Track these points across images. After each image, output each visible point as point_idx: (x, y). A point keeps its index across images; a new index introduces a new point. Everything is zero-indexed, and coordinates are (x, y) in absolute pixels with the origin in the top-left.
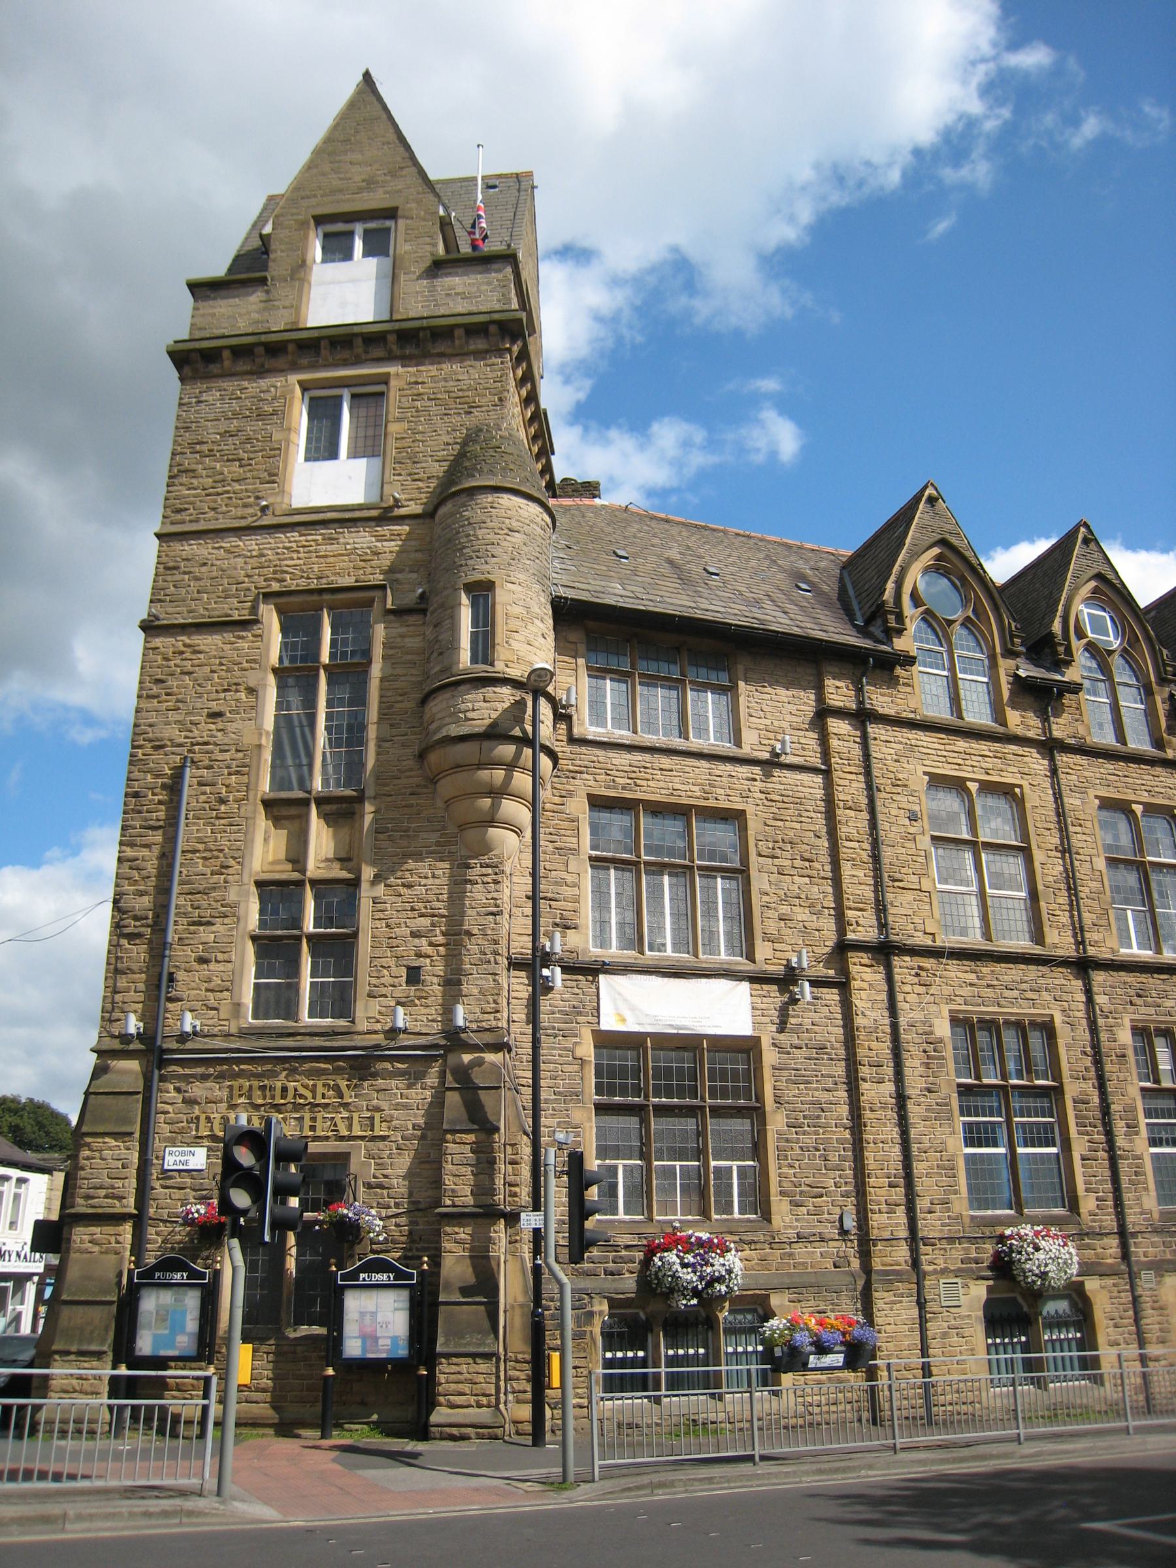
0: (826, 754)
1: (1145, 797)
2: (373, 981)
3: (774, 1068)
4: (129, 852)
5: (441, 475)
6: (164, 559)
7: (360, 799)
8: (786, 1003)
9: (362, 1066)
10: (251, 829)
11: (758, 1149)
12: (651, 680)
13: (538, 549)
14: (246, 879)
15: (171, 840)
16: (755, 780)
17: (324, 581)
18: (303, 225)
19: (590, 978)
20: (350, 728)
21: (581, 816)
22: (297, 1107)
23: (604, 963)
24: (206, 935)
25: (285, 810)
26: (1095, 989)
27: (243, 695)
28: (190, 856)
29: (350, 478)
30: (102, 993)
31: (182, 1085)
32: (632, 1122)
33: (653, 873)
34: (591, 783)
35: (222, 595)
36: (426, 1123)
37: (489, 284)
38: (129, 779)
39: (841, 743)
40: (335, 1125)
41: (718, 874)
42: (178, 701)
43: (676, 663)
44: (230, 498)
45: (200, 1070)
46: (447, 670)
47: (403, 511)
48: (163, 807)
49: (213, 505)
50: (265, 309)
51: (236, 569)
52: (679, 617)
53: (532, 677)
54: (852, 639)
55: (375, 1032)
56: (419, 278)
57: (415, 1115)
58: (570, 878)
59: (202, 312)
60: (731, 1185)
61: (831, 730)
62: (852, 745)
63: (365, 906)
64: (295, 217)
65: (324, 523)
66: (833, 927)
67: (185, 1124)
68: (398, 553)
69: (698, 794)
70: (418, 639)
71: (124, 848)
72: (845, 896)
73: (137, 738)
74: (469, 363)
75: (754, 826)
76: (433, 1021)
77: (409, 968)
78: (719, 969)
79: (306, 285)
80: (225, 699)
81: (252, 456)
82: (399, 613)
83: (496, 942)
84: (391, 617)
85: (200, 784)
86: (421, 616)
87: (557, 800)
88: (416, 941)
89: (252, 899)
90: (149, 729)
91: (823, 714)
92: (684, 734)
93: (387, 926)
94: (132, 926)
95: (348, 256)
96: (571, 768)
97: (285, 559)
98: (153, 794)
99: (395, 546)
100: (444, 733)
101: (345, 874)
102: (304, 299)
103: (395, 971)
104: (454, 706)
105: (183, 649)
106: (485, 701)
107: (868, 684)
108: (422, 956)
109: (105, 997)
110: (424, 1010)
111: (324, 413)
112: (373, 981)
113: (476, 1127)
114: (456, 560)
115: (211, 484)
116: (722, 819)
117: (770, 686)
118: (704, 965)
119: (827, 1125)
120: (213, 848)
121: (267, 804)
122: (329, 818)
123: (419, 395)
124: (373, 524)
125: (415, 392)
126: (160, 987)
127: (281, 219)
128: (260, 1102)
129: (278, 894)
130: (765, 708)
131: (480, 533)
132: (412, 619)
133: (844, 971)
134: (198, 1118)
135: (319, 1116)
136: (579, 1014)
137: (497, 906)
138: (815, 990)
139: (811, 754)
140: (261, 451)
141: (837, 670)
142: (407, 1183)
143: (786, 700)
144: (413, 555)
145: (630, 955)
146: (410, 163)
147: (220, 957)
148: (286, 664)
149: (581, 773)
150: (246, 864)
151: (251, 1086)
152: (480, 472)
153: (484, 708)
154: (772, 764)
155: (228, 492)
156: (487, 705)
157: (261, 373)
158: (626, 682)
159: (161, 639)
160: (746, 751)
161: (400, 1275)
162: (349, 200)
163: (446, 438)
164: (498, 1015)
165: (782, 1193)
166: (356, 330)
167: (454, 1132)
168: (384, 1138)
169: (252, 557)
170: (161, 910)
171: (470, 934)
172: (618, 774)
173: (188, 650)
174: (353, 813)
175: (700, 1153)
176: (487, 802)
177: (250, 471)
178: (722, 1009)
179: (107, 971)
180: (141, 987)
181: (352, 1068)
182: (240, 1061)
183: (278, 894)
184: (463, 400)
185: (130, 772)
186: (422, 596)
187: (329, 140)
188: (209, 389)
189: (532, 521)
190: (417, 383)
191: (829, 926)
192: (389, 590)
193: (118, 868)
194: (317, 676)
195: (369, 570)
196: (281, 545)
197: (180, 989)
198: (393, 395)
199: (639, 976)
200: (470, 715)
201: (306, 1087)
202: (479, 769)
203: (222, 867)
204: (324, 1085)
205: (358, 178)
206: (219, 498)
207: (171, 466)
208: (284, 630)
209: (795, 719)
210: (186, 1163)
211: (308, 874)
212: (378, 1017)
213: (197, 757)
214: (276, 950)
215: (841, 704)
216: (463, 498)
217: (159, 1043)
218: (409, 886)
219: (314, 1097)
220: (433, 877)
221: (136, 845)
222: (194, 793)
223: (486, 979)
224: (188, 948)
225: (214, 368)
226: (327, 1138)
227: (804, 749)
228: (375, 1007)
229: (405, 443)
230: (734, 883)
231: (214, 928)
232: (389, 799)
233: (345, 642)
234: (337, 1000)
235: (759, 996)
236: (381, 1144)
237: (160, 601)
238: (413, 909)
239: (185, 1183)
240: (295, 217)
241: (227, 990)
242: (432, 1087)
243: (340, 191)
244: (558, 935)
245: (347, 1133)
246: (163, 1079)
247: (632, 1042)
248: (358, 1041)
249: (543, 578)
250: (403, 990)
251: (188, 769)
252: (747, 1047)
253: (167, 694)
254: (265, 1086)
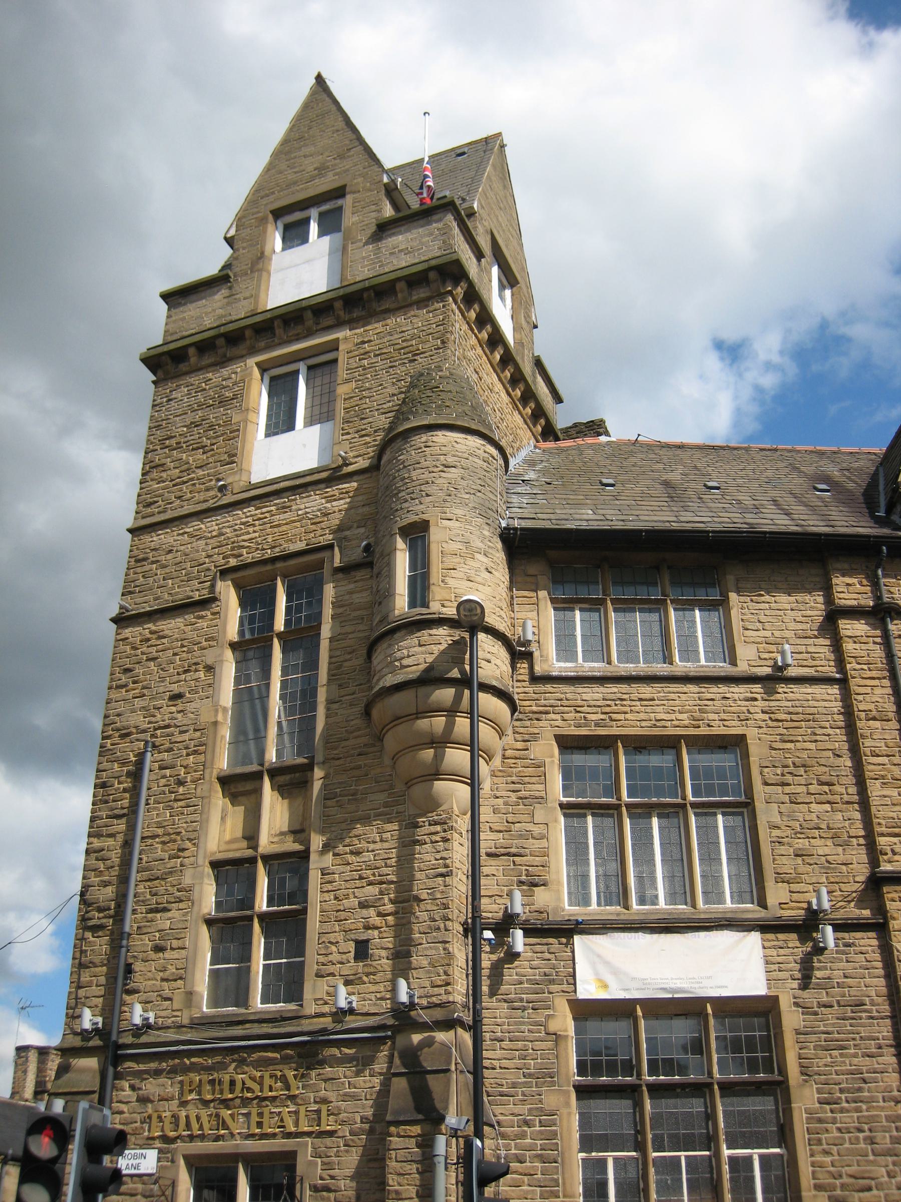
0: (840, 662)
2: (322, 959)
3: (798, 1032)
4: (97, 843)
5: (387, 426)
6: (136, 552)
7: (309, 767)
8: (809, 953)
9: (309, 1053)
10: (206, 810)
11: (784, 1134)
12: (624, 606)
13: (479, 482)
14: (200, 861)
15: (132, 827)
16: (756, 699)
17: (277, 549)
18: (263, 221)
19: (564, 940)
20: (303, 692)
21: (547, 760)
22: (245, 1102)
23: (578, 923)
24: (163, 922)
25: (240, 786)
27: (201, 674)
28: (150, 841)
29: (304, 445)
30: (68, 989)
31: (136, 1082)
32: (623, 1106)
33: (640, 816)
34: (560, 723)
35: (185, 578)
36: (374, 1115)
37: (431, 234)
38: (98, 771)
39: (857, 646)
40: (282, 1120)
41: (719, 811)
42: (144, 688)
43: (656, 584)
44: (194, 485)
45: (153, 1065)
46: (384, 619)
47: (351, 468)
48: (127, 795)
49: (180, 494)
50: (228, 304)
51: (198, 551)
52: (647, 531)
53: (462, 612)
54: (864, 528)
55: (323, 1015)
56: (366, 243)
57: (364, 1107)
58: (536, 830)
59: (174, 318)
60: (752, 1179)
61: (843, 633)
62: (871, 646)
63: (314, 878)
64: (255, 216)
65: (277, 493)
66: (864, 858)
67: (138, 1124)
68: (347, 510)
69: (686, 722)
70: (365, 594)
71: (92, 839)
72: (875, 821)
73: (107, 728)
74: (412, 313)
75: (757, 752)
76: (382, 999)
77: (357, 942)
78: (720, 919)
79: (264, 274)
80: (185, 681)
81: (214, 441)
82: (345, 570)
83: (446, 907)
84: (340, 575)
85: (162, 768)
86: (369, 570)
87: (520, 745)
88: (365, 912)
89: (206, 881)
90: (117, 719)
91: (834, 614)
92: (668, 659)
93: (336, 898)
94: (96, 918)
95: (304, 240)
96: (534, 708)
97: (243, 534)
98: (119, 783)
99: (342, 504)
100: (381, 684)
101: (297, 847)
102: (263, 287)
103: (343, 947)
104: (390, 655)
105: (149, 636)
106: (420, 645)
107: (885, 576)
108: (369, 928)
109: (70, 993)
110: (373, 988)
111: (282, 388)
112: (322, 959)
113: (420, 1117)
114: (393, 505)
115: (178, 475)
116: (720, 747)
117: (768, 593)
118: (702, 916)
119: (869, 1101)
120: (171, 831)
121: (225, 781)
122: (282, 790)
123: (366, 353)
124: (323, 486)
125: (362, 351)
126: (120, 978)
127: (244, 220)
128: (209, 1097)
129: (232, 871)
130: (763, 618)
131: (414, 474)
132: (360, 574)
133: (881, 910)
134: (150, 1117)
135: (266, 1111)
136: (552, 982)
137: (446, 866)
138: (840, 935)
139: (822, 663)
140: (222, 435)
141: (846, 566)
142: (354, 1184)
143: (788, 606)
144: (361, 510)
145: (613, 911)
146: (357, 143)
147: (175, 943)
148: (248, 636)
149: (547, 713)
150: (201, 845)
151: (200, 1081)
152: (415, 414)
153: (418, 653)
154: (776, 678)
155: (192, 479)
156: (423, 649)
157: (224, 362)
158: (598, 610)
159: (130, 629)
160: (743, 667)
162: (302, 189)
163: (391, 390)
164: (449, 988)
165: (818, 1187)
166: (304, 304)
167: (397, 1123)
168: (331, 1134)
169: (213, 537)
170: (121, 899)
171: (418, 900)
172: (590, 710)
173: (154, 636)
174: (306, 782)
175: (710, 1141)
176: (428, 754)
177: (212, 456)
178: (732, 966)
179: (73, 966)
180: (102, 980)
181: (300, 1056)
182: (190, 1054)
183: (232, 871)
184: (407, 350)
185: (99, 763)
186: (367, 548)
187: (285, 142)
188: (179, 386)
189: (471, 454)
190: (363, 342)
191: (859, 857)
192: (336, 549)
193: (86, 860)
194: (271, 647)
195: (318, 533)
196: (238, 522)
197: (138, 980)
198: (342, 357)
199: (622, 935)
200: (405, 662)
201: (253, 1079)
202: (418, 718)
203: (180, 850)
204: (271, 1077)
205: (311, 168)
206: (184, 487)
207: (144, 464)
208: (243, 604)
209: (804, 626)
210: (137, 1167)
211: (261, 850)
212: (326, 998)
213: (158, 741)
214: (230, 930)
215: (855, 603)
216: (399, 443)
217: (114, 1038)
218: (357, 853)
219: (261, 1091)
220: (382, 841)
221: (102, 836)
222: (155, 777)
223: (437, 949)
224: (146, 937)
225: (183, 367)
226: (274, 1135)
227: (813, 659)
228: (323, 987)
229: (353, 402)
230: (739, 819)
231: (169, 914)
232: (338, 762)
233: (299, 609)
234: (288, 983)
235: (774, 947)
236: (328, 1141)
237: (130, 593)
238: (361, 878)
239: (136, 1189)
240: (255, 216)
241: (181, 978)
242: (381, 1074)
243: (295, 183)
244: (518, 895)
245: (293, 1129)
246: (118, 1076)
247: (620, 1010)
248: (307, 1025)
249: (486, 512)
250: (352, 967)
251: (149, 754)
252: (763, 1010)
253: (134, 682)
254: (214, 1080)
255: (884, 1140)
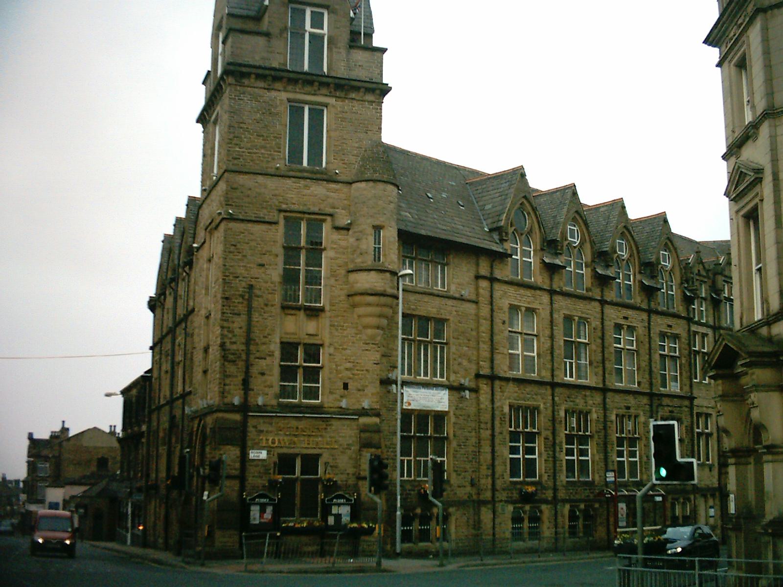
0: (478, 295)
1: (580, 314)
26: (556, 395)
161: (348, 500)
210: (259, 456)
214: (288, 373)
228: (332, 397)
255: (470, 457)
